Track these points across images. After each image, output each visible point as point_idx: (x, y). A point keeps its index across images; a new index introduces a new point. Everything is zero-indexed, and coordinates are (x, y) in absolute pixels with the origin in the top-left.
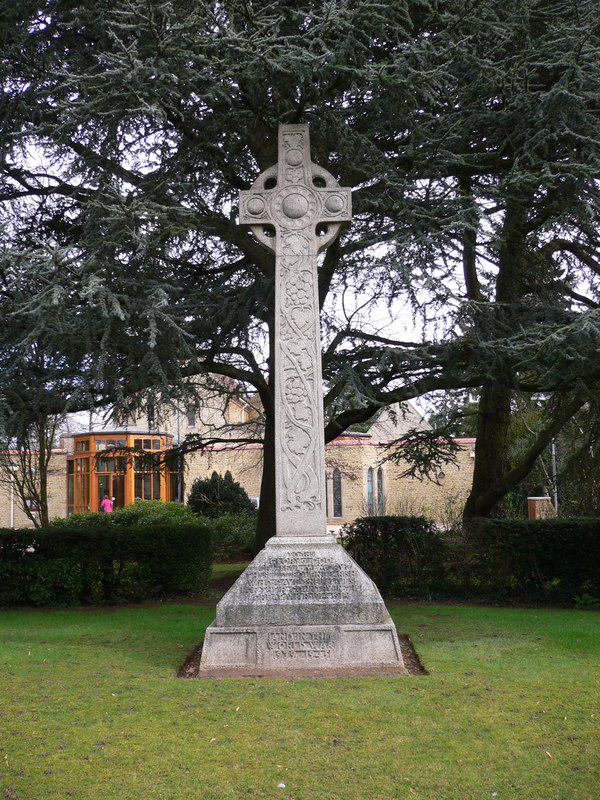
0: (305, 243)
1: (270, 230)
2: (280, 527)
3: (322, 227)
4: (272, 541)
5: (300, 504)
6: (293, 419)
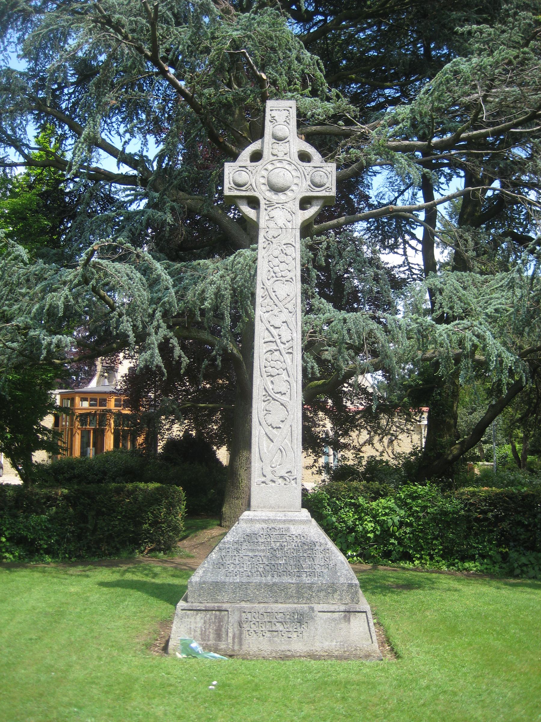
0: (289, 217)
1: (254, 202)
2: (254, 502)
3: (305, 203)
4: (246, 514)
5: (275, 479)
6: (271, 393)
